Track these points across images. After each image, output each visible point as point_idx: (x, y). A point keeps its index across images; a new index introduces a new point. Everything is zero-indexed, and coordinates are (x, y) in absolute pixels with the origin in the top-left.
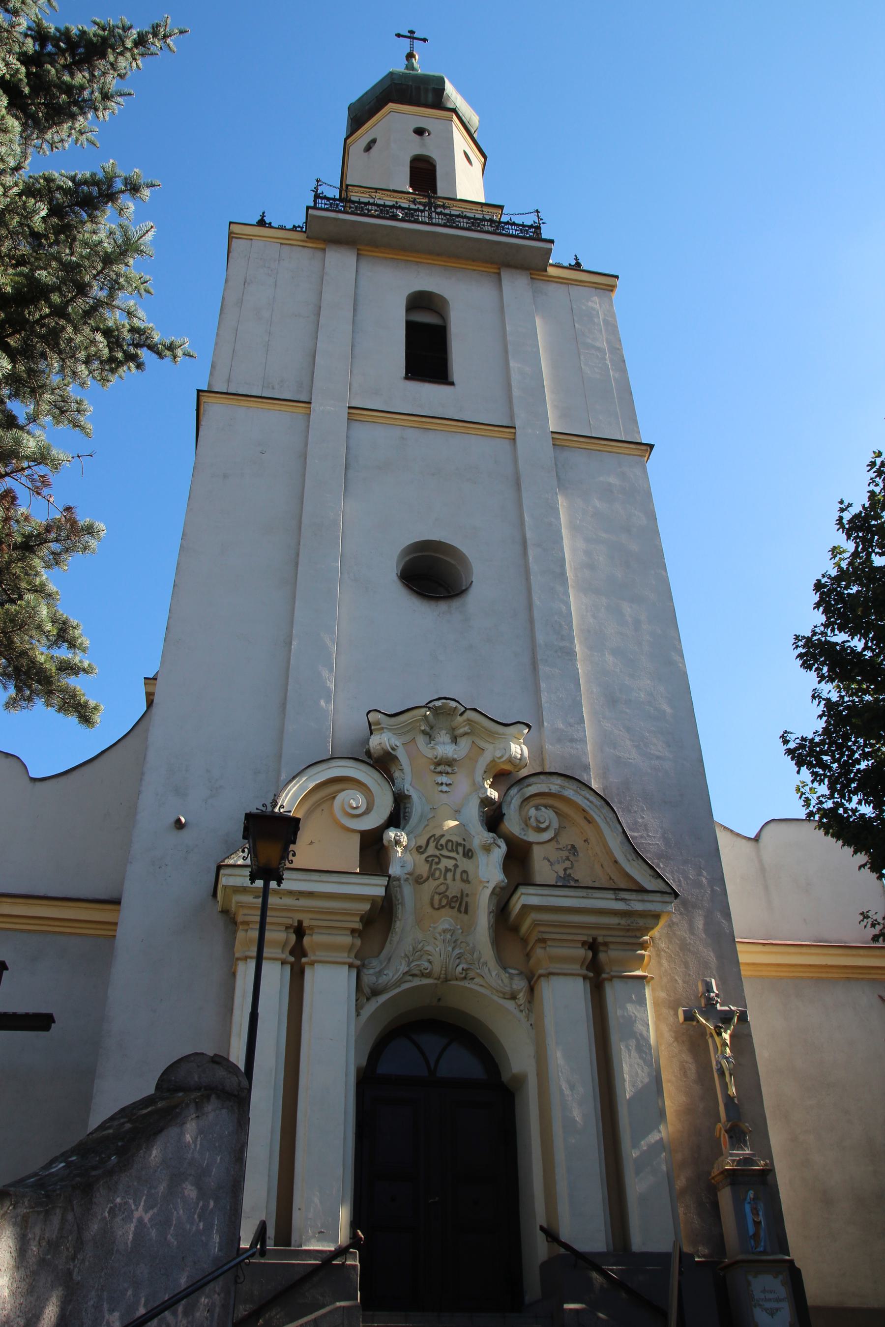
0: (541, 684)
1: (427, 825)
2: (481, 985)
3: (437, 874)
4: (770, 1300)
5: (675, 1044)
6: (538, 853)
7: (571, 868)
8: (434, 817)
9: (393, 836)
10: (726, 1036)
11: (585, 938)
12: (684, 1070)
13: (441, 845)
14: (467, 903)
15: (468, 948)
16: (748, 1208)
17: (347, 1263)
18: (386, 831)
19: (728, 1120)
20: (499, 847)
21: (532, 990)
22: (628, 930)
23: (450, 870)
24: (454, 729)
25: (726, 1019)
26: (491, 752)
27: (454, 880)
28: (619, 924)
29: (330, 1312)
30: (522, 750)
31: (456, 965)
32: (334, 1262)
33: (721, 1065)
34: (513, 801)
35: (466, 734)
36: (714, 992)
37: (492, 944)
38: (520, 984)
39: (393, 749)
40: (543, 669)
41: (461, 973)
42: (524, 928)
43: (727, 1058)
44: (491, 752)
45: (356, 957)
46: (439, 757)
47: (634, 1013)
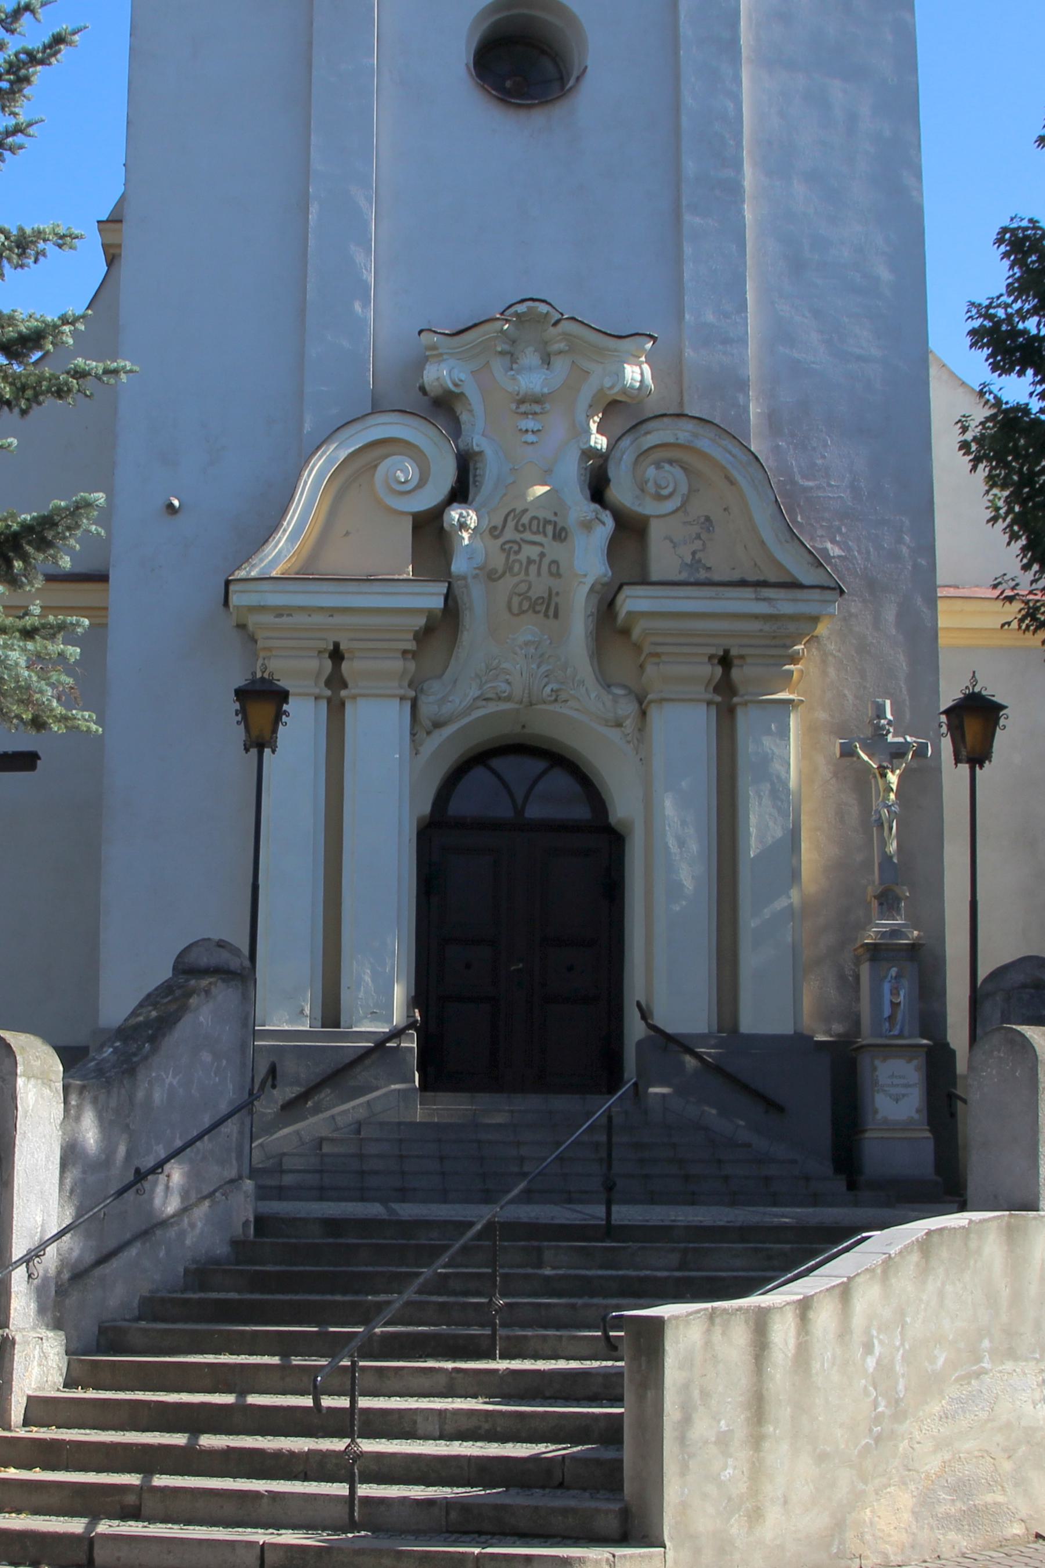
0: (685, 249)
1: (505, 495)
2: (576, 710)
3: (517, 566)
4: (898, 1085)
5: (833, 781)
6: (656, 532)
7: (703, 550)
8: (514, 482)
9: (457, 517)
10: (893, 778)
11: (712, 651)
12: (841, 814)
13: (523, 525)
14: (557, 605)
15: (558, 663)
16: (887, 987)
17: (402, 1045)
18: (446, 511)
19: (881, 884)
20: (604, 524)
21: (644, 713)
22: (774, 637)
23: (534, 561)
24: (546, 343)
25: (898, 753)
26: (597, 380)
27: (539, 574)
28: (761, 630)
29: (385, 1095)
30: (642, 374)
31: (543, 685)
32: (388, 1045)
33: (880, 816)
34: (624, 457)
35: (560, 352)
36: (885, 718)
37: (591, 657)
38: (628, 708)
39: (456, 385)
40: (687, 217)
41: (551, 696)
42: (636, 633)
43: (888, 807)
44: (597, 380)
45: (410, 685)
46: (522, 393)
47: (770, 749)
